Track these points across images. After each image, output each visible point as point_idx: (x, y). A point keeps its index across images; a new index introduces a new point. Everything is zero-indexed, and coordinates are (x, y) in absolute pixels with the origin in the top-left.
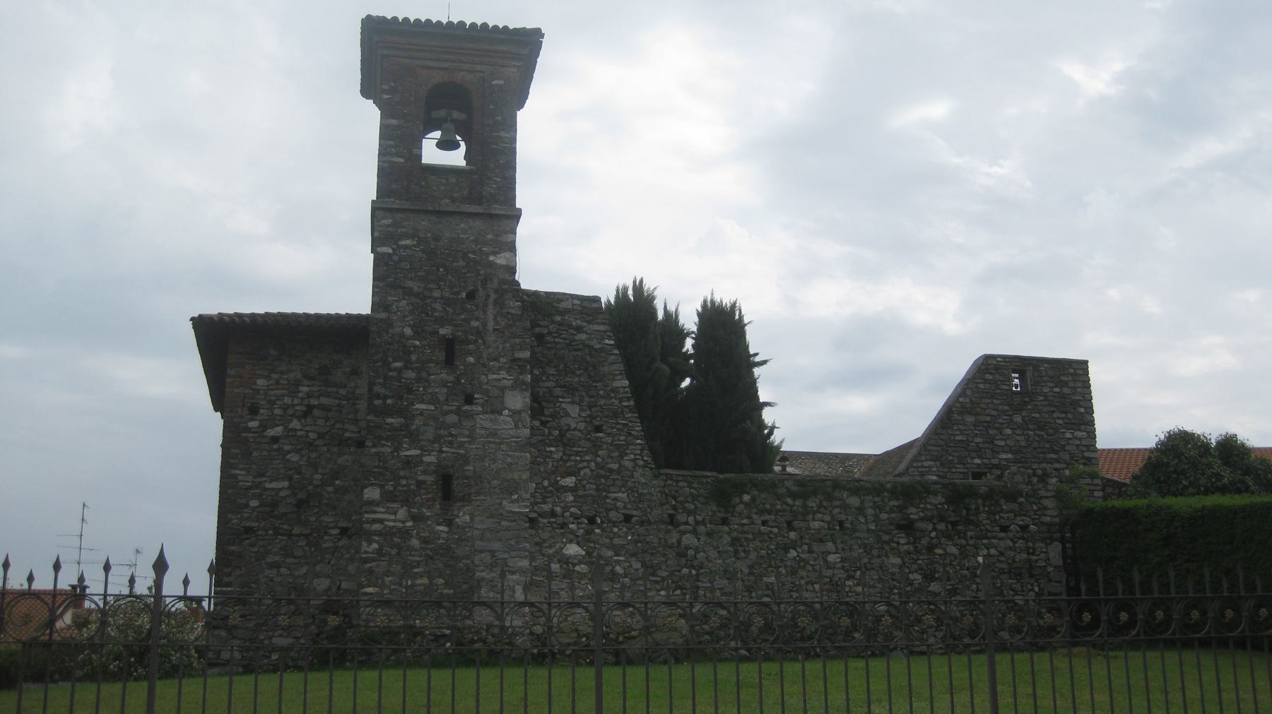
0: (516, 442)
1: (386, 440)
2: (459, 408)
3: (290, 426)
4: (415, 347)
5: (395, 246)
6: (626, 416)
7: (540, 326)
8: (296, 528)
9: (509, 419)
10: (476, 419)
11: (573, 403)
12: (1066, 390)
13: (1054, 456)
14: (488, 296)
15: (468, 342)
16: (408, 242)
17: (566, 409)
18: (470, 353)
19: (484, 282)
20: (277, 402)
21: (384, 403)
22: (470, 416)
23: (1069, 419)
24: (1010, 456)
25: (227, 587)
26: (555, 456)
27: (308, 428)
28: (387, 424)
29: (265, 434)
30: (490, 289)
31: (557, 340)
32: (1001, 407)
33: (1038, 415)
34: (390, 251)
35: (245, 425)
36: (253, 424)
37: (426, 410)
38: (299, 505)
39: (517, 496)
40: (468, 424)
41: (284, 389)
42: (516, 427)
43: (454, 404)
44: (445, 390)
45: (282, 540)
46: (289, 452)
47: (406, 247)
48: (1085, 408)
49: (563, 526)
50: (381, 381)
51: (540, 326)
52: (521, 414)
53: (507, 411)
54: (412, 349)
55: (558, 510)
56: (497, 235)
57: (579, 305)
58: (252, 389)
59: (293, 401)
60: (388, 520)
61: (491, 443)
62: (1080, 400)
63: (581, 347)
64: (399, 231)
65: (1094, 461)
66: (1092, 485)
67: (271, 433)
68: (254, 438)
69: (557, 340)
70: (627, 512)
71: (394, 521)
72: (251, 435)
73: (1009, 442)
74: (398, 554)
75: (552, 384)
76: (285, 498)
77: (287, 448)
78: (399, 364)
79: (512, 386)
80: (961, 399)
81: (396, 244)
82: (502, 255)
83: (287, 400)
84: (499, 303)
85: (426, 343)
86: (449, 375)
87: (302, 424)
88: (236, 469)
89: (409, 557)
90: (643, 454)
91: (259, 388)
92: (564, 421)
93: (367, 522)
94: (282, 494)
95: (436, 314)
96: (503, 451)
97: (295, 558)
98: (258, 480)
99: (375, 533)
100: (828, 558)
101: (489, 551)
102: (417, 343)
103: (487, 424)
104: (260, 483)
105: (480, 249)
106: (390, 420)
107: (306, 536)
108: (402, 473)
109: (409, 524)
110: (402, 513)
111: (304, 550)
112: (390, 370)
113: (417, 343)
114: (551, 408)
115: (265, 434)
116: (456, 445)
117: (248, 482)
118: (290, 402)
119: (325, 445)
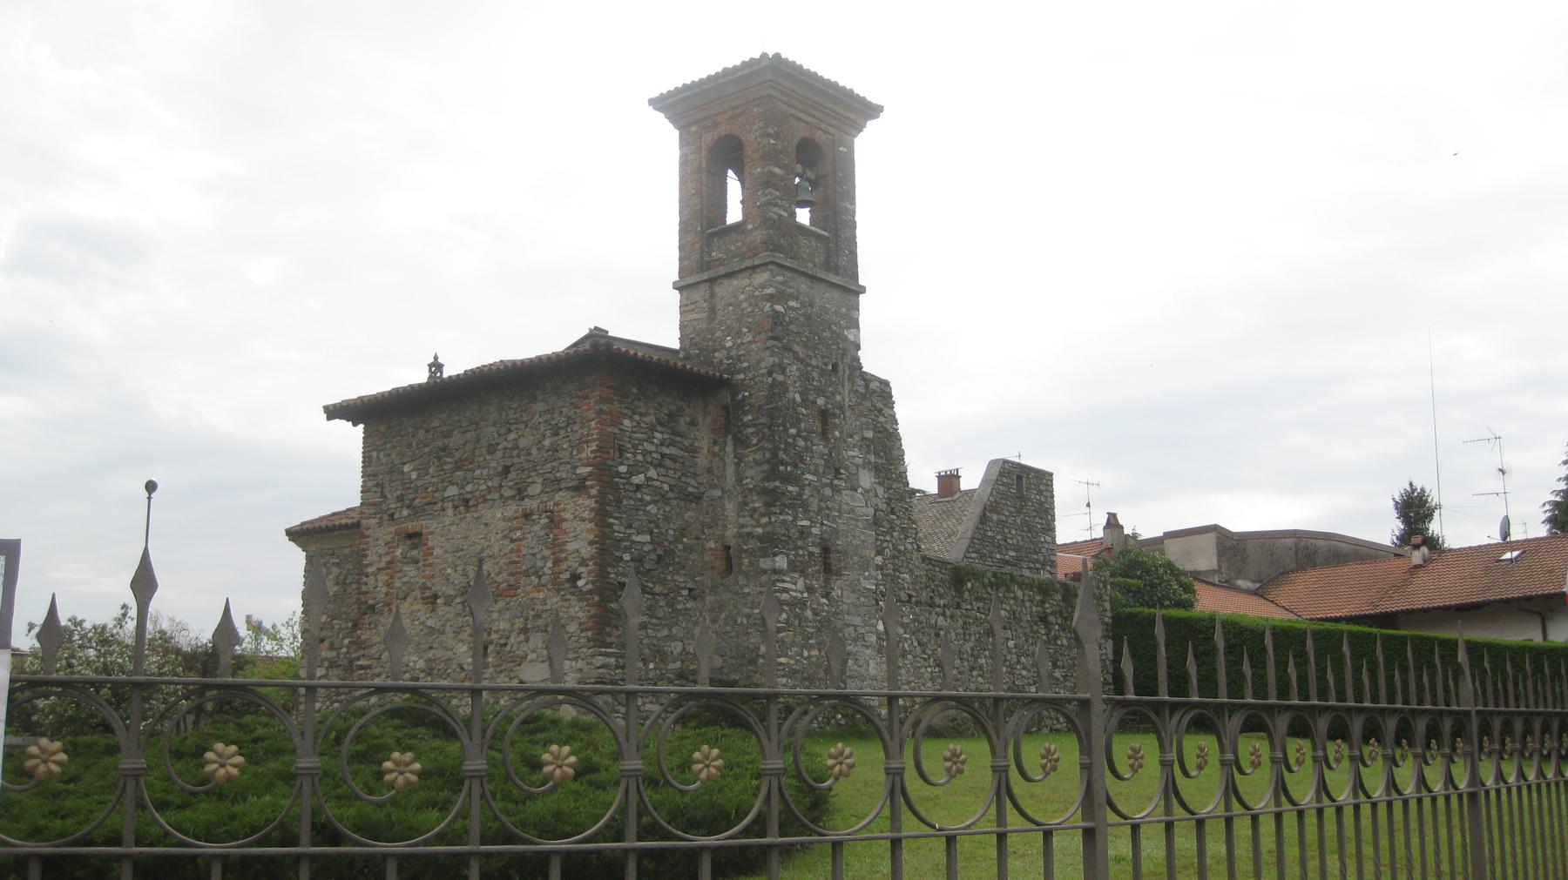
1: (789, 508)
8: (657, 586)
12: (1043, 499)
15: (835, 416)
35: (616, 469)
38: (660, 558)
45: (648, 599)
54: (801, 417)
58: (620, 429)
60: (793, 590)
63: (881, 429)
68: (624, 484)
72: (621, 481)
78: (793, 431)
81: (786, 303)
84: (851, 379)
93: (779, 591)
98: (628, 531)
107: (666, 595)
109: (806, 595)
110: (801, 584)
119: (676, 498)
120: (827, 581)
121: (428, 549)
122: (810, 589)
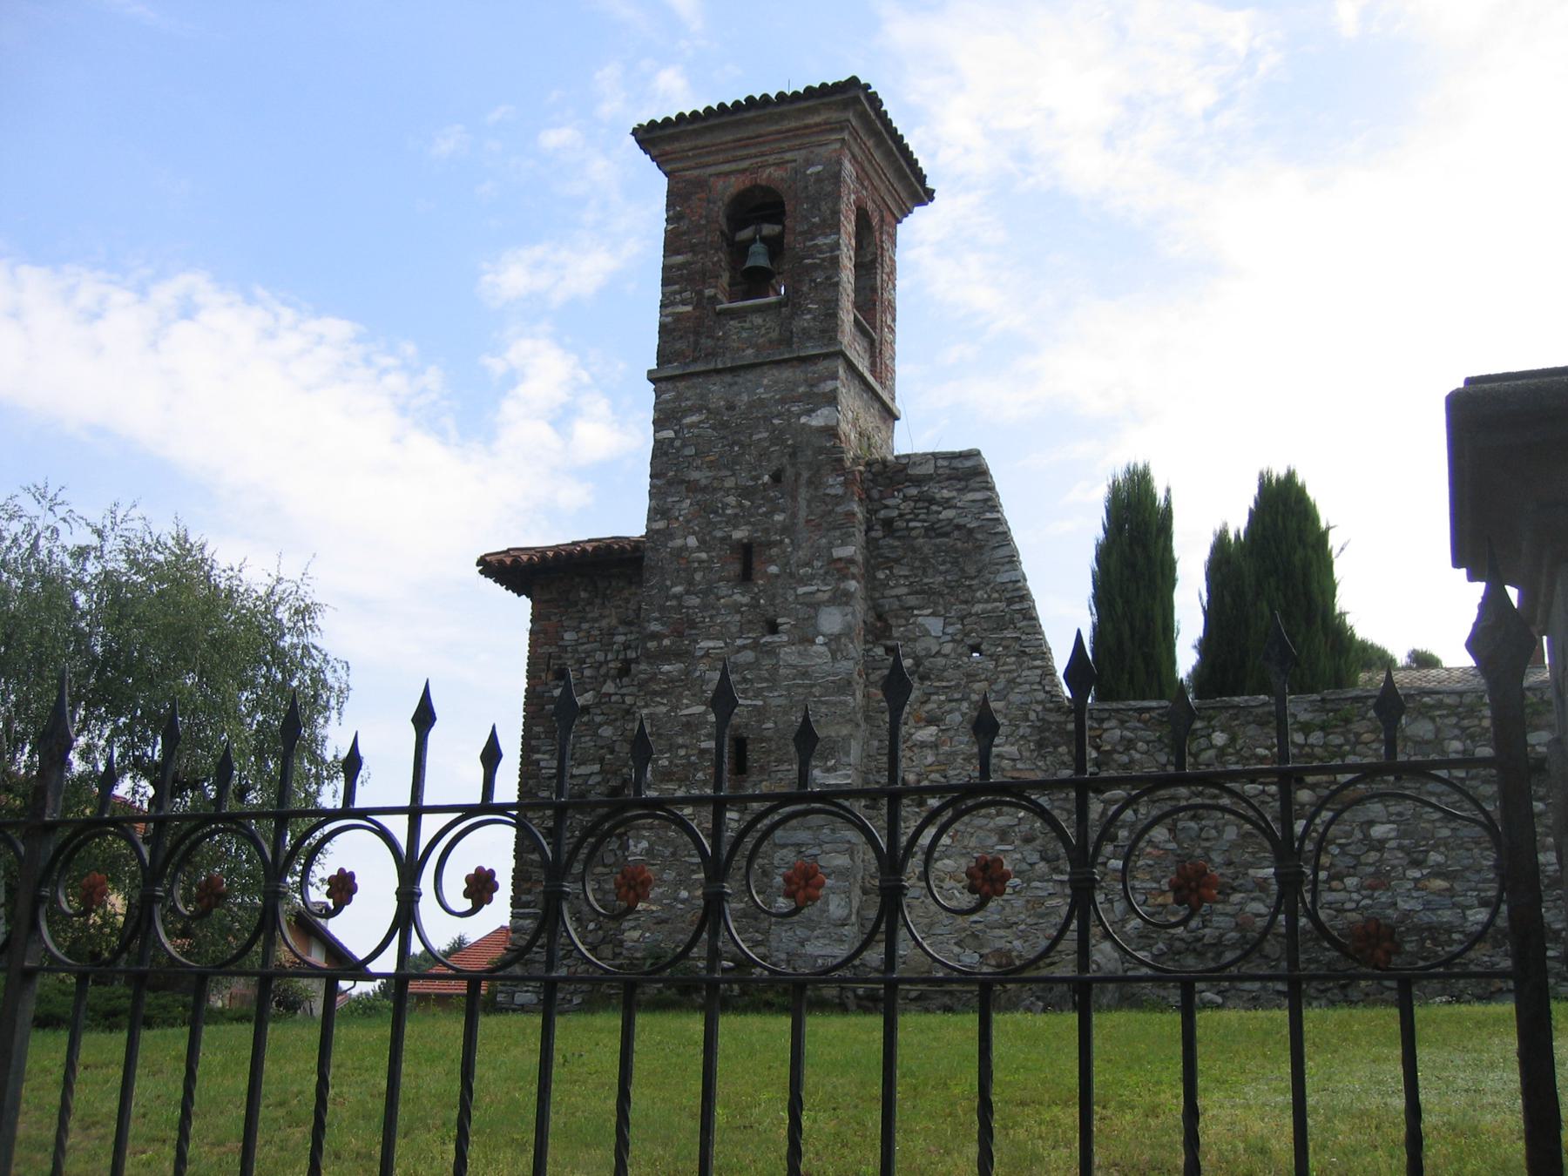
0: (833, 682)
2: (756, 641)
3: (603, 691)
4: (701, 562)
5: (677, 428)
6: (1018, 625)
7: (887, 507)
10: (779, 654)
11: (933, 614)
14: (798, 475)
15: (770, 545)
16: (695, 418)
17: (923, 625)
18: (771, 561)
19: (793, 455)
20: (588, 660)
21: (660, 645)
22: (772, 651)
25: (524, 908)
27: (624, 691)
28: (662, 673)
30: (801, 463)
31: (912, 524)
37: (714, 648)
39: (833, 761)
40: (767, 662)
41: (596, 641)
42: (834, 658)
43: (750, 635)
44: (738, 617)
46: (600, 725)
50: (656, 615)
51: (887, 507)
52: (840, 639)
53: (821, 637)
56: (812, 386)
57: (946, 467)
59: (606, 656)
61: (799, 686)
63: (948, 529)
64: (683, 405)
69: (912, 524)
74: (673, 854)
75: (902, 591)
76: (594, 786)
77: (598, 719)
78: (678, 589)
79: (828, 601)
82: (819, 412)
83: (599, 656)
85: (714, 554)
86: (744, 596)
87: (616, 686)
88: (538, 752)
89: (687, 859)
90: (1043, 682)
91: (566, 643)
94: (592, 781)
95: (729, 512)
96: (815, 697)
97: (605, 866)
100: (1372, 833)
102: (704, 556)
103: (794, 660)
105: (788, 410)
106: (666, 668)
108: (680, 741)
111: (616, 855)
112: (668, 598)
113: (704, 556)
114: (900, 626)
116: (751, 694)
117: (552, 768)
118: (602, 659)
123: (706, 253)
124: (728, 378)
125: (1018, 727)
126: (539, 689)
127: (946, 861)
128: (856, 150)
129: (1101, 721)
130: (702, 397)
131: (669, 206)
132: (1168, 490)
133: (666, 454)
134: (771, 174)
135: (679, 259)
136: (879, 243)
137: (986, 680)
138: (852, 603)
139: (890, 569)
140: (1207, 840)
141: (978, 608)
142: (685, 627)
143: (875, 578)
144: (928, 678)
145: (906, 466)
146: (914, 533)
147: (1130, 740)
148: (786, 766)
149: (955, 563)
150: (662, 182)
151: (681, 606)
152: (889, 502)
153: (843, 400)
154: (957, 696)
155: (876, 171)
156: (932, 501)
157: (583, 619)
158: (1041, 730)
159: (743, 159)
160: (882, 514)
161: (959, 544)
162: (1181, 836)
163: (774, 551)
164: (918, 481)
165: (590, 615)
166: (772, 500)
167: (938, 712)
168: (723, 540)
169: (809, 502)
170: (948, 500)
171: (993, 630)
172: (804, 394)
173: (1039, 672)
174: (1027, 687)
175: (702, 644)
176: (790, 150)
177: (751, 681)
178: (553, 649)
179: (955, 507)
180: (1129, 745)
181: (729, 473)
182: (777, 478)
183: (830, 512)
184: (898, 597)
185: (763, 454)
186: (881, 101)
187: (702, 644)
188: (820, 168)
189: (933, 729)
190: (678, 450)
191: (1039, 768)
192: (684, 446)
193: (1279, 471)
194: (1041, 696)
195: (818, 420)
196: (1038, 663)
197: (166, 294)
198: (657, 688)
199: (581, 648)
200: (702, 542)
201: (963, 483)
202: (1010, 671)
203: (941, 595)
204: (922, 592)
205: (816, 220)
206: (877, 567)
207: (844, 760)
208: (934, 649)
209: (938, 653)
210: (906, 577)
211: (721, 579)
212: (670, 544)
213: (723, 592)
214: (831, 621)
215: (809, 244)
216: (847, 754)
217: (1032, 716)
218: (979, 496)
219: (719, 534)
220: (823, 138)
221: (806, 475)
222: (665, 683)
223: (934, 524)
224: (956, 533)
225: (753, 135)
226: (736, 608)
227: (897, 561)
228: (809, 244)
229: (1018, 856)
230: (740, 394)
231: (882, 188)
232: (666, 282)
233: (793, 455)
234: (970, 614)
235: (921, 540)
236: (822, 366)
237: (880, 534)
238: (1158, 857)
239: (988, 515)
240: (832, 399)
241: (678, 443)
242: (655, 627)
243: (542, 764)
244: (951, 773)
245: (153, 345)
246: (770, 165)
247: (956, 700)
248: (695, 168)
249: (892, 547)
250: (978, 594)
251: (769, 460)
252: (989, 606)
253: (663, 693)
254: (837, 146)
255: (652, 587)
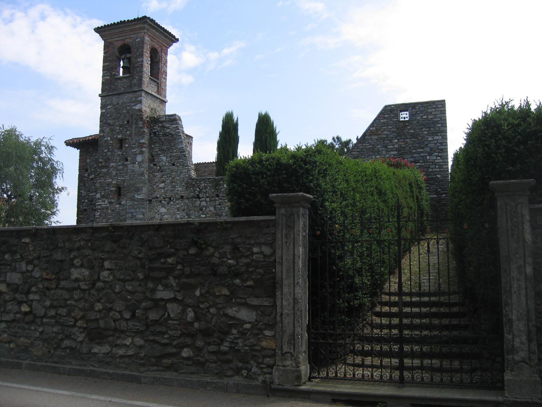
2: (123, 163)
4: (111, 144)
7: (154, 129)
9: (137, 165)
11: (164, 156)
13: (422, 150)
14: (133, 122)
15: (126, 139)
18: (127, 144)
19: (132, 116)
23: (431, 131)
24: (396, 152)
26: (158, 176)
29: (89, 178)
31: (160, 133)
32: (392, 130)
33: (413, 131)
34: (105, 111)
36: (86, 175)
40: (125, 169)
44: (119, 158)
47: (109, 109)
48: (442, 124)
49: (161, 202)
51: (154, 129)
55: (158, 196)
60: (102, 204)
61: (132, 174)
62: (439, 120)
63: (168, 134)
65: (444, 150)
66: (443, 162)
67: (91, 177)
68: (86, 179)
69: (160, 133)
70: (181, 195)
71: (104, 204)
73: (395, 146)
74: (105, 215)
78: (106, 151)
79: (139, 153)
80: (371, 129)
88: (82, 190)
92: (161, 164)
95: (117, 131)
98: (88, 193)
99: (99, 209)
101: (131, 213)
102: (112, 142)
103: (131, 168)
104: (88, 194)
105: (131, 105)
106: (103, 170)
108: (106, 188)
110: (106, 202)
113: (112, 142)
115: (89, 178)
116: (122, 176)
120: (119, 199)
121: (335, 141)
122: (110, 203)
123: (113, 63)
124: (117, 96)
125: (182, 183)
126: (81, 174)
127: (166, 216)
128: (150, 33)
129: (200, 182)
130: (111, 101)
131: (104, 49)
132: (237, 118)
133: (103, 116)
134: (128, 41)
135: (106, 64)
136: (160, 55)
137: (175, 172)
138: (144, 154)
139: (155, 144)
140: (222, 210)
141: (174, 154)
142: (107, 160)
143: (151, 147)
144: (163, 172)
145: (159, 118)
146: (160, 135)
147: (206, 186)
148: (129, 194)
149: (169, 143)
150: (102, 43)
151: (106, 155)
152: (155, 128)
153: (144, 102)
154: (169, 176)
155: (157, 37)
156: (165, 127)
157: (92, 156)
158: (187, 184)
159: (121, 37)
160: (153, 131)
161: (170, 138)
162: (216, 209)
163: (127, 141)
164: (162, 122)
165: (93, 155)
166: (127, 128)
167: (165, 180)
168: (116, 138)
169: (135, 128)
170: (168, 127)
171: (177, 160)
172: (135, 101)
173: (187, 170)
174: (184, 174)
175: (111, 164)
176: (132, 34)
177: (122, 173)
178: (84, 164)
179: (170, 129)
180: (206, 187)
181: (117, 121)
182: (128, 122)
183: (139, 131)
184: (156, 152)
185: (125, 116)
186: (155, 20)
187: (111, 164)
188: (139, 40)
189: (163, 184)
190: (106, 115)
191: (186, 193)
192: (107, 114)
193: (263, 113)
194: (187, 176)
195: (137, 107)
196: (187, 168)
197: (34, 12)
198: (101, 175)
199: (91, 163)
200: (111, 139)
201: (172, 123)
202: (181, 170)
203: (166, 151)
204: (162, 150)
205: (138, 54)
206: (152, 144)
207: (142, 192)
208: (164, 164)
209: (165, 165)
210: (158, 146)
211: (115, 148)
212: (104, 139)
213: (116, 151)
214: (139, 158)
215: (136, 60)
216: (142, 191)
217: (185, 181)
218: (175, 126)
219: (115, 137)
220: (140, 31)
221: (134, 121)
222: (103, 174)
223: (165, 133)
224: (170, 135)
225: (123, 30)
226: (119, 155)
227: (156, 142)
228: (136, 60)
229: (181, 214)
230: (120, 100)
231: (161, 41)
232: (103, 70)
233: (132, 116)
234: (172, 156)
235: (162, 137)
236: (138, 93)
237: (153, 136)
238: (211, 214)
239: (177, 131)
240: (140, 102)
241: (106, 113)
242: (101, 160)
243: (83, 193)
244: (167, 195)
245: (33, 31)
246: (128, 38)
247: (169, 177)
248: (110, 39)
249: (156, 139)
250: (174, 151)
251: (126, 118)
252: (176, 154)
253: (102, 177)
254: (143, 33)
255: (100, 150)
